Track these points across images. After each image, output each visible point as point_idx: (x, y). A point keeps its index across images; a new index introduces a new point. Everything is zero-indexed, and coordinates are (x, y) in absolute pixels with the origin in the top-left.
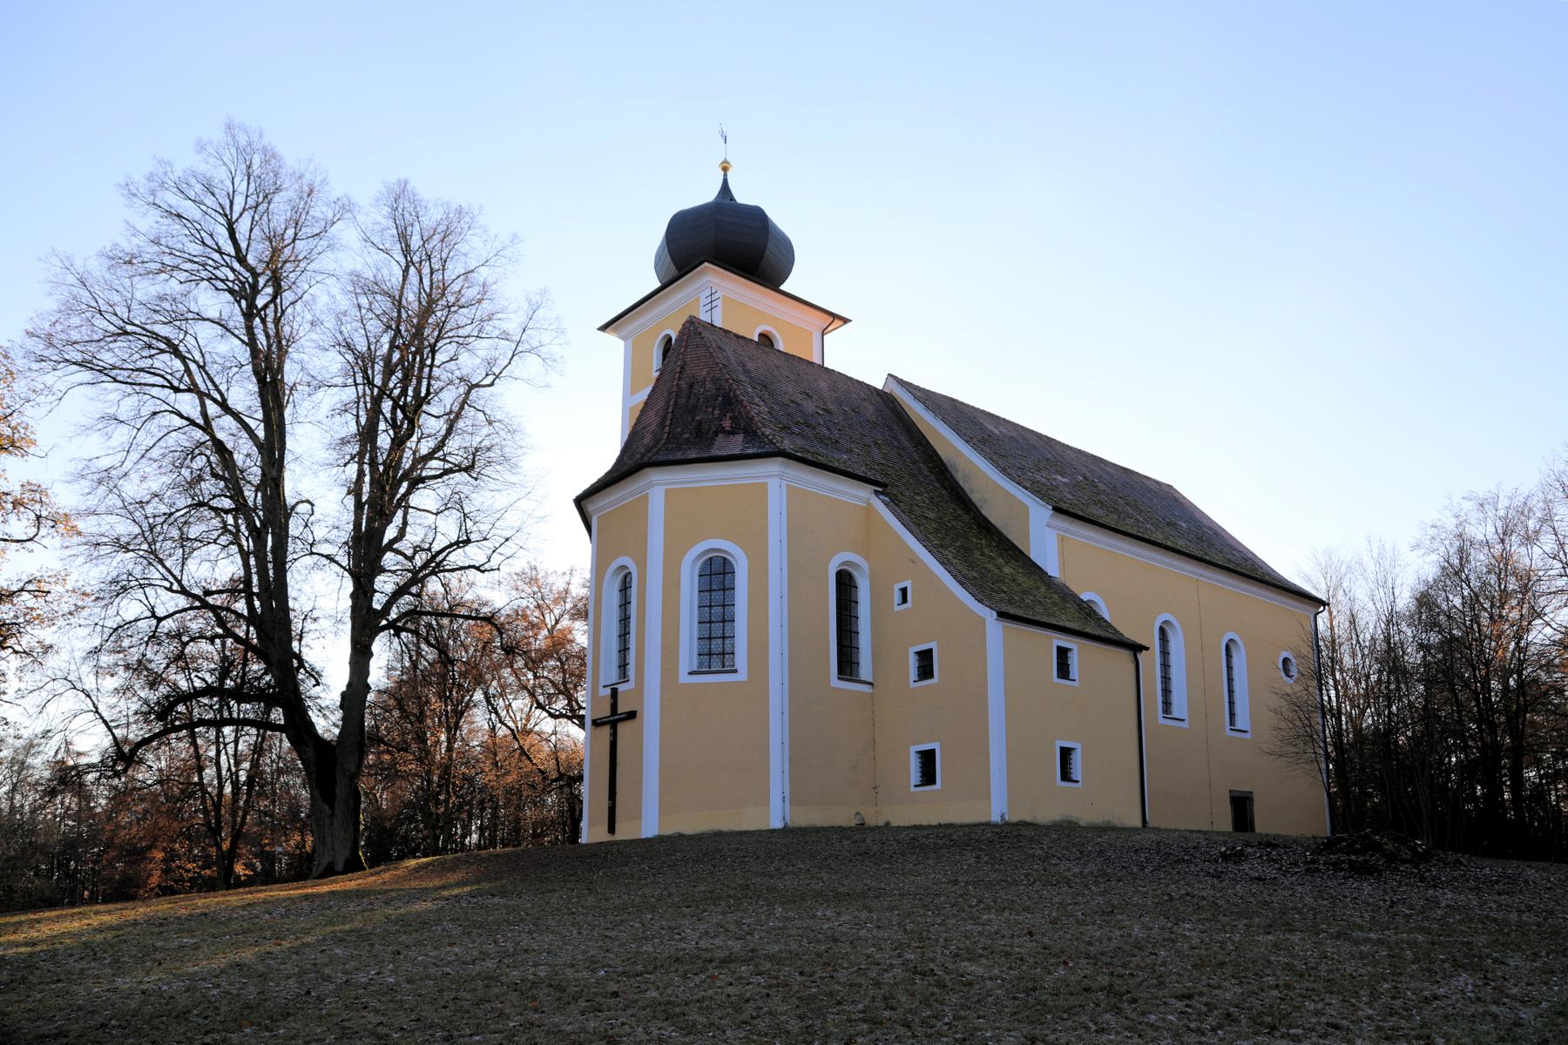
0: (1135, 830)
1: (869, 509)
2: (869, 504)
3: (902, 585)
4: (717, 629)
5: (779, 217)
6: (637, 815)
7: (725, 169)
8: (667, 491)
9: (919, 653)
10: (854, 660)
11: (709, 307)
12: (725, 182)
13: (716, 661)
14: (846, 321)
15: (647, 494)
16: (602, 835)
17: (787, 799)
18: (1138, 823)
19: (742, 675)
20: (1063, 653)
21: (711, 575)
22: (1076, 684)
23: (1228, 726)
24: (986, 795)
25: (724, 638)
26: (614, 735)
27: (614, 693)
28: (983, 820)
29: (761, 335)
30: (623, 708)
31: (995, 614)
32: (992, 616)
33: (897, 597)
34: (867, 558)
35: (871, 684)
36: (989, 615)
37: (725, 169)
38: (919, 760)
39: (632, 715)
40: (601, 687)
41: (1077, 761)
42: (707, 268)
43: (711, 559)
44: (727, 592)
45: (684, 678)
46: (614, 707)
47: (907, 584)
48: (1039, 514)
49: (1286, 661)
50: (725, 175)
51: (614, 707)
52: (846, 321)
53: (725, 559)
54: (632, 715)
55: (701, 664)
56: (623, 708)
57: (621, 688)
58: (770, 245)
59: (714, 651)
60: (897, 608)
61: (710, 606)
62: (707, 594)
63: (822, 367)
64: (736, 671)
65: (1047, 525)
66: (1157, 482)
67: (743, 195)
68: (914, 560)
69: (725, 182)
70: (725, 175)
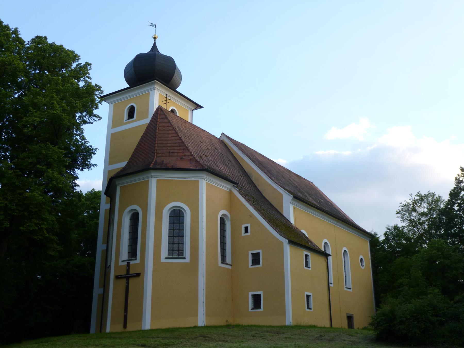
0: (328, 328)
1: (231, 192)
2: (230, 190)
3: (246, 225)
4: (176, 240)
5: (179, 64)
6: (140, 318)
7: (155, 38)
8: (157, 180)
9: (253, 254)
10: (224, 255)
11: (165, 102)
12: (155, 44)
13: (176, 253)
14: (201, 107)
15: (148, 181)
16: (119, 328)
17: (205, 314)
18: (328, 325)
19: (187, 260)
20: (306, 256)
21: (174, 217)
22: (310, 269)
23: (345, 287)
24: (283, 313)
25: (179, 243)
26: (128, 283)
27: (128, 264)
28: (282, 324)
29: (171, 110)
30: (132, 271)
31: (287, 241)
32: (286, 242)
33: (243, 230)
34: (230, 213)
35: (231, 265)
36: (285, 241)
37: (155, 38)
38: (252, 299)
39: (138, 275)
40: (120, 261)
41: (312, 299)
42: (155, 83)
43: (174, 210)
44: (181, 224)
45: (163, 260)
46: (128, 271)
47: (249, 225)
48: (287, 198)
49: (361, 259)
50: (155, 41)
51: (128, 271)
52: (201, 107)
53: (180, 210)
54: (138, 275)
55: (169, 254)
56: (132, 271)
57: (132, 262)
58: (175, 74)
59: (175, 249)
60: (243, 235)
61: (174, 230)
62: (172, 224)
63: (191, 124)
64: (184, 258)
65: (290, 203)
66: (308, 181)
67: (163, 50)
68: (252, 216)
69: (155, 44)
70: (155, 41)
